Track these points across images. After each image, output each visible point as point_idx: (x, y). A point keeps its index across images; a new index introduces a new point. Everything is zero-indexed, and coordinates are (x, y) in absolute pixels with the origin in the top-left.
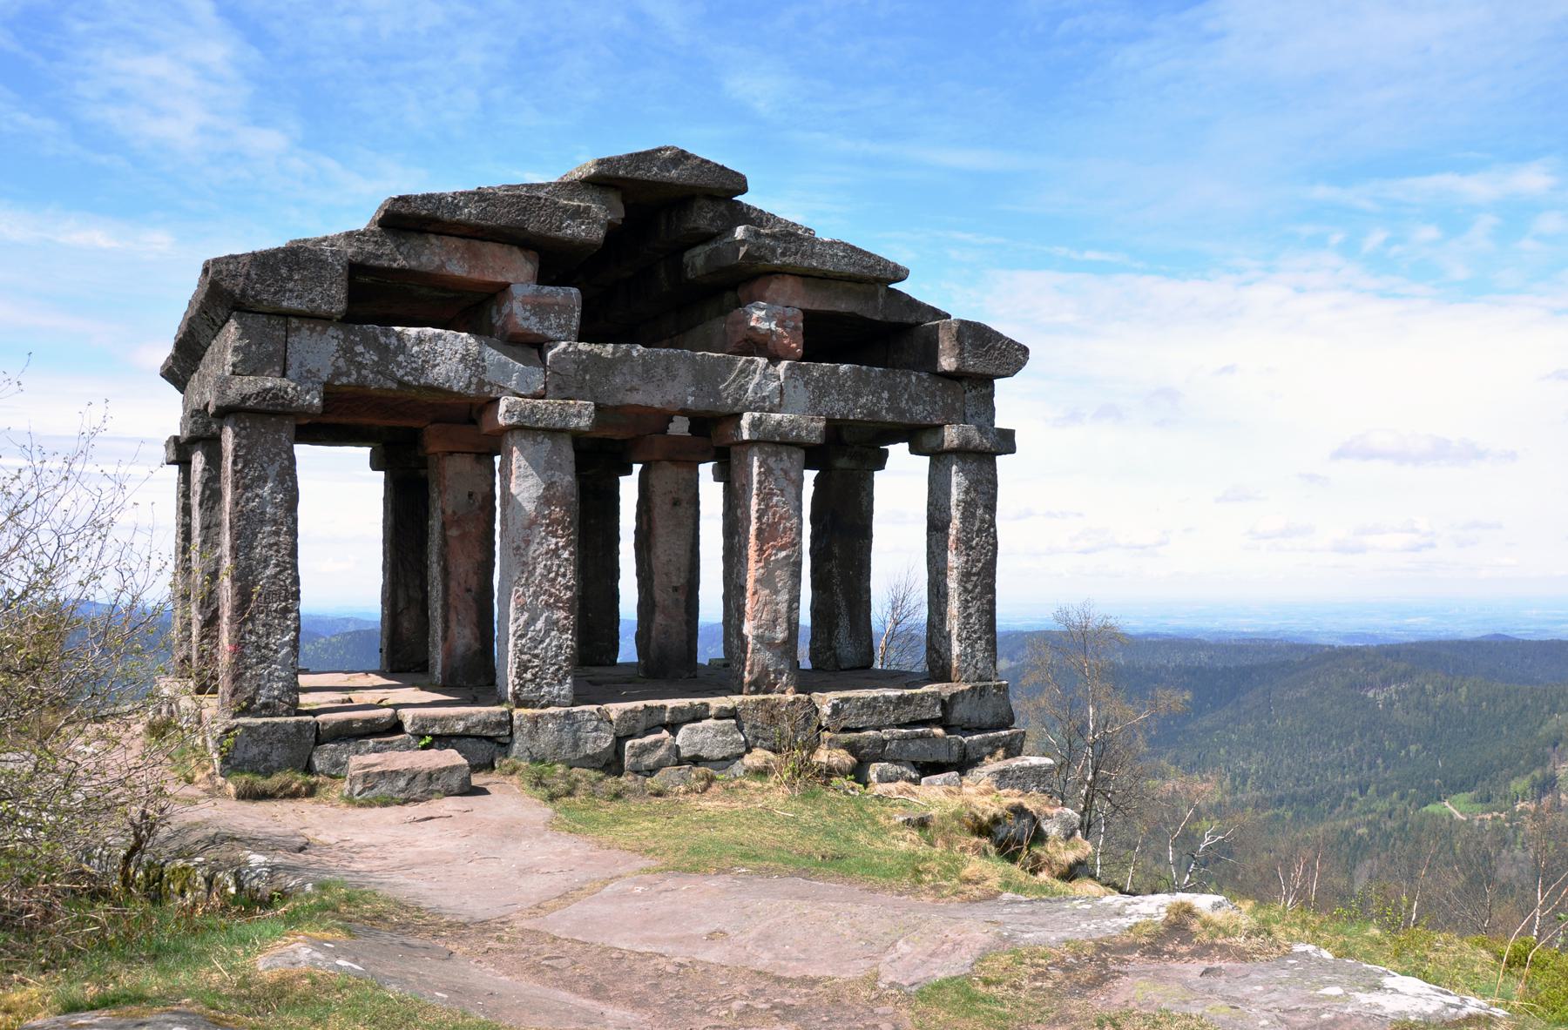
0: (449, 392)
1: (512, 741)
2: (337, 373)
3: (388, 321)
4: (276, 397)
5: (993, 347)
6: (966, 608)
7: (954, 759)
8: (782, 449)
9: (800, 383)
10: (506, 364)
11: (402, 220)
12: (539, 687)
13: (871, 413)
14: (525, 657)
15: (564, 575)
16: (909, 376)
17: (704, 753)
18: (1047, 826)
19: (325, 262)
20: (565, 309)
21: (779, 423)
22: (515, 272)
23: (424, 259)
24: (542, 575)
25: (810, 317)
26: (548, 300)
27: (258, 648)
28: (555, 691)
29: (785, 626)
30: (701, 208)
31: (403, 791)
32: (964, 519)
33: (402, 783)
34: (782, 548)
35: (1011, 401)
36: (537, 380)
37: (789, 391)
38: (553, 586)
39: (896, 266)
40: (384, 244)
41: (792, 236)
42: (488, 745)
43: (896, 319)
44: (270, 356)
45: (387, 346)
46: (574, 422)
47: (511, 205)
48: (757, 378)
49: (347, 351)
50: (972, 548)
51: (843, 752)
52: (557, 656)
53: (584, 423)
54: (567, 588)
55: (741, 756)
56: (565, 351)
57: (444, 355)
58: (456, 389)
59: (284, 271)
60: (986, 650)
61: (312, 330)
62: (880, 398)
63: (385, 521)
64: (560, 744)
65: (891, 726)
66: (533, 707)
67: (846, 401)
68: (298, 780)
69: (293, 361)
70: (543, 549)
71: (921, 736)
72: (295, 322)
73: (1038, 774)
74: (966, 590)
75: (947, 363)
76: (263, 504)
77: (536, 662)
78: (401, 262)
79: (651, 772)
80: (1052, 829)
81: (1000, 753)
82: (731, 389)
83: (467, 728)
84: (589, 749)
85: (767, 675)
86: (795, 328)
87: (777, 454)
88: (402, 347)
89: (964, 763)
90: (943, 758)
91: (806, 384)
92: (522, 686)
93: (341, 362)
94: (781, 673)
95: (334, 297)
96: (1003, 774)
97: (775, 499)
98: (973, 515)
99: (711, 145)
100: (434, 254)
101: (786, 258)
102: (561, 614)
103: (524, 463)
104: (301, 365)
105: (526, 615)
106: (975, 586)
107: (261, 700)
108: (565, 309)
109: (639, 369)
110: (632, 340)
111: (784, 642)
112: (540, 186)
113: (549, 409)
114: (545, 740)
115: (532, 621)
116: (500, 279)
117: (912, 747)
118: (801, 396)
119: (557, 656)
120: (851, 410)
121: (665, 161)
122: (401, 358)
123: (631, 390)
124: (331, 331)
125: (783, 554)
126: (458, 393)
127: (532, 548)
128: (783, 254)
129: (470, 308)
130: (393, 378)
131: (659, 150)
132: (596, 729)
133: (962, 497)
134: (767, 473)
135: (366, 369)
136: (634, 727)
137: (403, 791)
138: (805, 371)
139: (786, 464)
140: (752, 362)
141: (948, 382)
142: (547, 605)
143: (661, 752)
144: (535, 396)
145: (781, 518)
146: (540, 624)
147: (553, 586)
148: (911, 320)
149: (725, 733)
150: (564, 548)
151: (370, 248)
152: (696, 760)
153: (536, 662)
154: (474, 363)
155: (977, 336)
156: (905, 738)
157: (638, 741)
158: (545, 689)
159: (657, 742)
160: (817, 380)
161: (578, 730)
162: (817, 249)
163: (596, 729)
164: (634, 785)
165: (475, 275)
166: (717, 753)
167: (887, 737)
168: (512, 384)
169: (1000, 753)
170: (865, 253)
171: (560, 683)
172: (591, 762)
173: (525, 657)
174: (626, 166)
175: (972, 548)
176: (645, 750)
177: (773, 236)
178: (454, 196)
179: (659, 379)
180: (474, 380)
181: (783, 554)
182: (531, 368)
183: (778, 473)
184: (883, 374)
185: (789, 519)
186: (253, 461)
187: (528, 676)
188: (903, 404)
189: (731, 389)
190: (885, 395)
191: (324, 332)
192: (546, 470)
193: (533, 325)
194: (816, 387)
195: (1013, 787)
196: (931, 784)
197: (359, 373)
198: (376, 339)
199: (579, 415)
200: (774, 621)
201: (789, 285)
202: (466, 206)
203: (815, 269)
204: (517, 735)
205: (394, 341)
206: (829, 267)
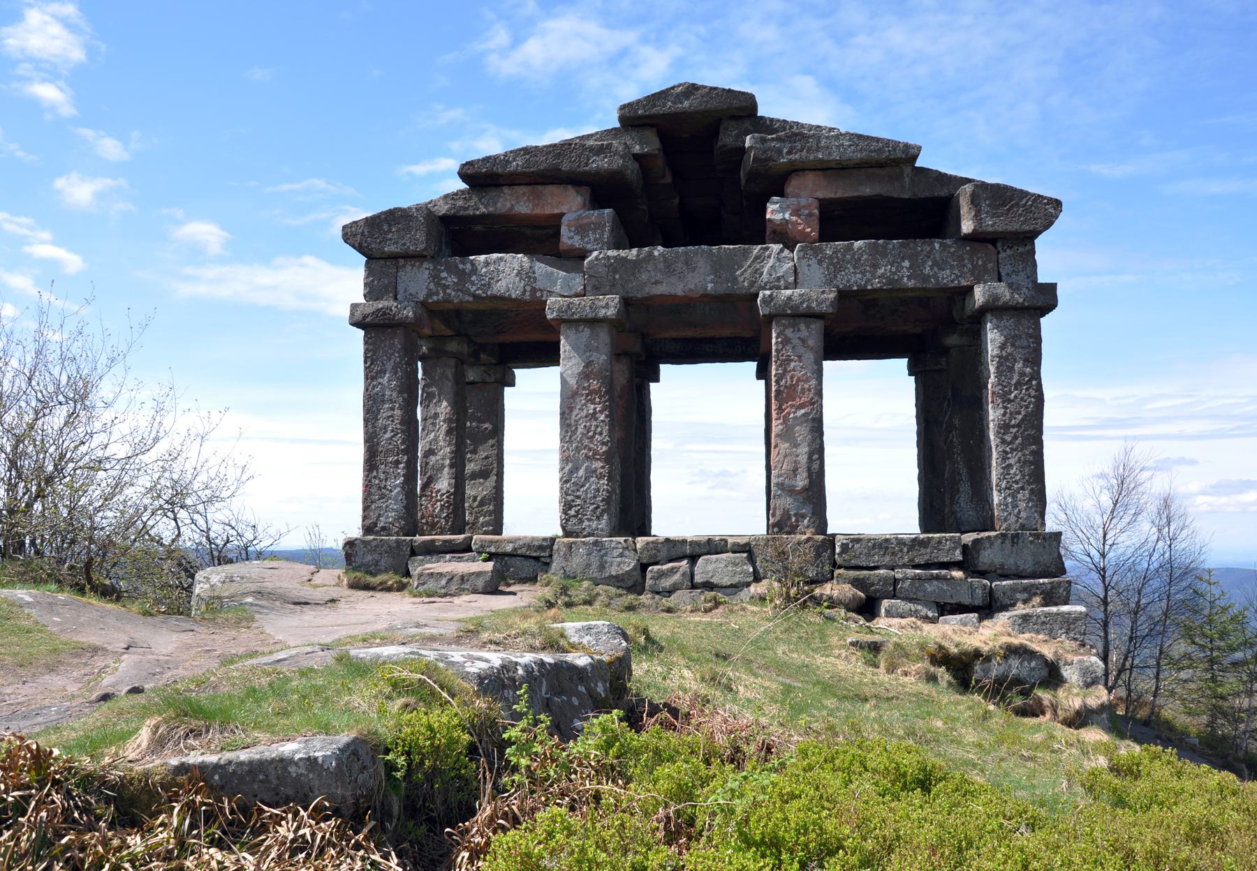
0: (509, 299)
1: (552, 561)
2: (430, 294)
3: (465, 252)
4: (384, 314)
5: (1017, 204)
6: (1004, 459)
7: (978, 602)
8: (797, 320)
9: (813, 262)
10: (552, 273)
11: (481, 177)
12: (581, 521)
13: (891, 281)
14: (570, 498)
15: (601, 434)
16: (931, 244)
17: (715, 580)
18: (1066, 672)
19: (412, 216)
20: (599, 226)
21: (789, 298)
22: (569, 206)
23: (499, 205)
24: (583, 434)
26: (585, 221)
27: (380, 488)
28: (594, 525)
29: (805, 474)
30: (727, 129)
31: (443, 588)
32: (999, 373)
33: (443, 582)
34: (801, 406)
35: (1052, 257)
36: (578, 282)
37: (803, 270)
38: (592, 442)
39: (907, 146)
40: (470, 198)
41: (794, 133)
42: (533, 562)
43: (926, 194)
44: (386, 287)
45: (464, 270)
46: (602, 313)
47: (548, 153)
48: (771, 261)
49: (435, 277)
50: (1010, 401)
51: (847, 587)
52: (595, 497)
53: (611, 312)
54: (603, 443)
55: (748, 585)
56: (597, 258)
57: (505, 272)
58: (514, 296)
59: (385, 227)
60: (1030, 500)
61: (413, 266)
62: (900, 268)
63: (918, 455)
64: (588, 565)
65: (904, 566)
66: (577, 536)
67: (863, 273)
68: (391, 579)
69: (401, 289)
70: (584, 413)
71: (938, 578)
72: (402, 262)
73: (1068, 623)
74: (1003, 442)
75: (967, 226)
76: (383, 389)
77: (579, 502)
78: (483, 210)
79: (669, 592)
80: (1070, 674)
81: (1037, 600)
82: (747, 275)
83: (515, 549)
84: (614, 571)
85: (789, 518)
86: (810, 215)
88: (474, 270)
89: (987, 608)
90: (966, 600)
91: (820, 262)
92: (568, 520)
93: (432, 286)
94: (804, 517)
95: (417, 240)
96: (1026, 618)
97: (793, 364)
98: (1011, 369)
99: (721, 74)
100: (506, 200)
101: (801, 155)
102: (599, 464)
103: (568, 348)
104: (406, 291)
105: (570, 465)
106: (1015, 438)
107: (380, 525)
108: (599, 226)
109: (661, 266)
110: (652, 243)
111: (805, 489)
112: (589, 136)
113: (583, 306)
114: (577, 561)
115: (575, 469)
116: (556, 211)
117: (930, 587)
118: (814, 273)
119: (595, 497)
120: (868, 281)
121: (678, 95)
122: (474, 278)
123: (656, 283)
124: (426, 265)
125: (803, 411)
126: (516, 299)
127: (575, 413)
128: (789, 153)
129: (539, 238)
130: (468, 292)
131: (673, 88)
132: (621, 555)
133: (996, 352)
134: (786, 342)
135: (450, 290)
136: (655, 555)
137: (443, 588)
138: (817, 251)
139: (804, 333)
140: (767, 249)
141: (976, 245)
142: (587, 457)
143: (677, 577)
144: (577, 295)
145: (799, 380)
146: (581, 472)
147: (592, 442)
148: (943, 193)
149: (736, 565)
150: (601, 412)
151: (460, 203)
152: (709, 586)
153: (579, 502)
154: (527, 276)
155: (998, 197)
156: (918, 578)
157: (656, 568)
158: (586, 523)
159: (673, 568)
160: (831, 258)
161: (605, 555)
162: (823, 144)
163: (621, 555)
164: (648, 602)
165: (538, 211)
166: (726, 581)
167: (899, 576)
168: (557, 288)
169: (1037, 600)
170: (872, 139)
171: (598, 518)
172: (617, 581)
173: (570, 498)
174: (644, 106)
175: (1010, 401)
176: (662, 575)
177: (779, 139)
178: (506, 155)
179: (684, 272)
180: (528, 288)
181: (803, 411)
182: (572, 275)
183: (796, 341)
184: (901, 245)
185: (807, 381)
186: (377, 360)
187: (572, 512)
188: (927, 270)
189: (747, 275)
190: (906, 264)
191: (421, 266)
192: (585, 352)
193: (577, 242)
194: (831, 263)
195: (1038, 632)
196: (946, 622)
197: (445, 292)
198: (457, 267)
199: (607, 307)
200: (795, 471)
201: (810, 179)
202: (514, 160)
203: (821, 160)
204: (555, 557)
205: (469, 266)
206: (835, 156)
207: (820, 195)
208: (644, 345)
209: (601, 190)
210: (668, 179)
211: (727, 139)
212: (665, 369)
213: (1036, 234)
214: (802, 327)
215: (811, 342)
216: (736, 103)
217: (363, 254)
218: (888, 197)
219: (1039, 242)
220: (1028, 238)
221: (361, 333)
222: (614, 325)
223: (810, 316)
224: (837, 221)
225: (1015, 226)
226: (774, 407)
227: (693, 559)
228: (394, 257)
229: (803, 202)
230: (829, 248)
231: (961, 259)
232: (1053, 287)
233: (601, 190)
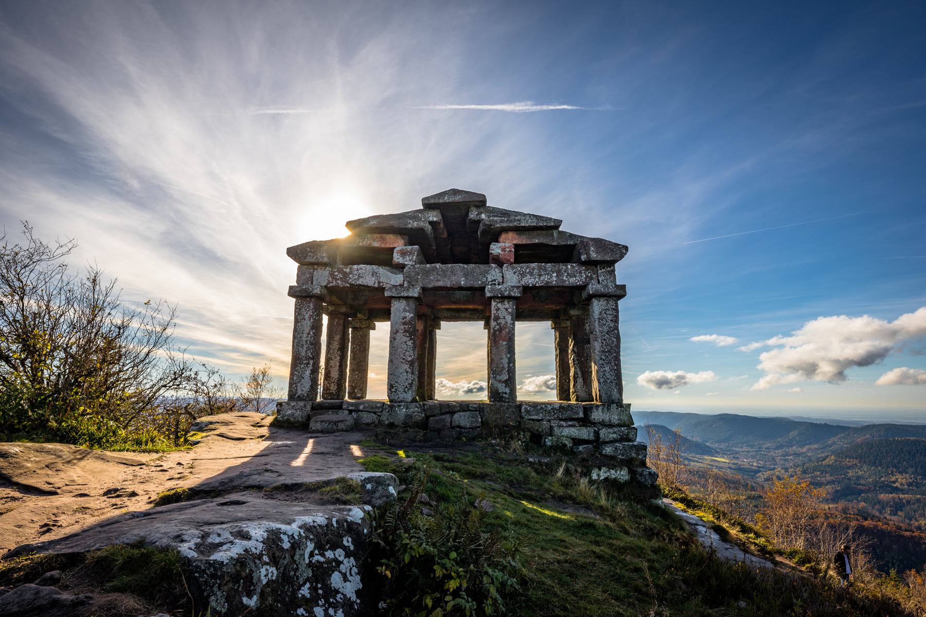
13: (547, 282)
20: (411, 253)
22: (399, 244)
25: (517, 246)
62: (551, 277)
87: (502, 302)
101: (512, 222)
108: (411, 253)
139: (507, 306)
155: (600, 243)
165: (383, 246)
179: (457, 275)
190: (555, 275)
193: (401, 261)
207: (515, 242)
208: (432, 310)
209: (413, 236)
210: (445, 235)
211: (473, 215)
212: (443, 323)
213: (615, 261)
214: (506, 303)
215: (510, 310)
216: (476, 199)
217: (295, 260)
218: (545, 243)
219: (616, 265)
220: (612, 263)
221: (294, 300)
222: (418, 299)
223: (510, 298)
224: (523, 255)
225: (607, 258)
226: (571, 357)
227: (453, 413)
228: (312, 264)
229: (507, 245)
230: (518, 267)
231: (580, 273)
232: (624, 286)
233: (413, 236)
